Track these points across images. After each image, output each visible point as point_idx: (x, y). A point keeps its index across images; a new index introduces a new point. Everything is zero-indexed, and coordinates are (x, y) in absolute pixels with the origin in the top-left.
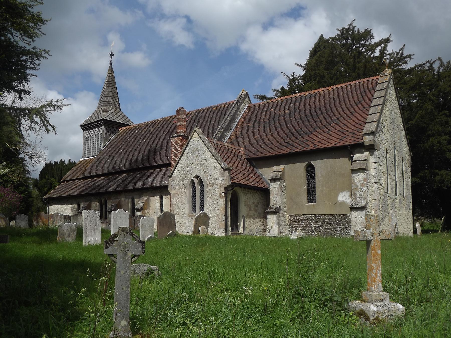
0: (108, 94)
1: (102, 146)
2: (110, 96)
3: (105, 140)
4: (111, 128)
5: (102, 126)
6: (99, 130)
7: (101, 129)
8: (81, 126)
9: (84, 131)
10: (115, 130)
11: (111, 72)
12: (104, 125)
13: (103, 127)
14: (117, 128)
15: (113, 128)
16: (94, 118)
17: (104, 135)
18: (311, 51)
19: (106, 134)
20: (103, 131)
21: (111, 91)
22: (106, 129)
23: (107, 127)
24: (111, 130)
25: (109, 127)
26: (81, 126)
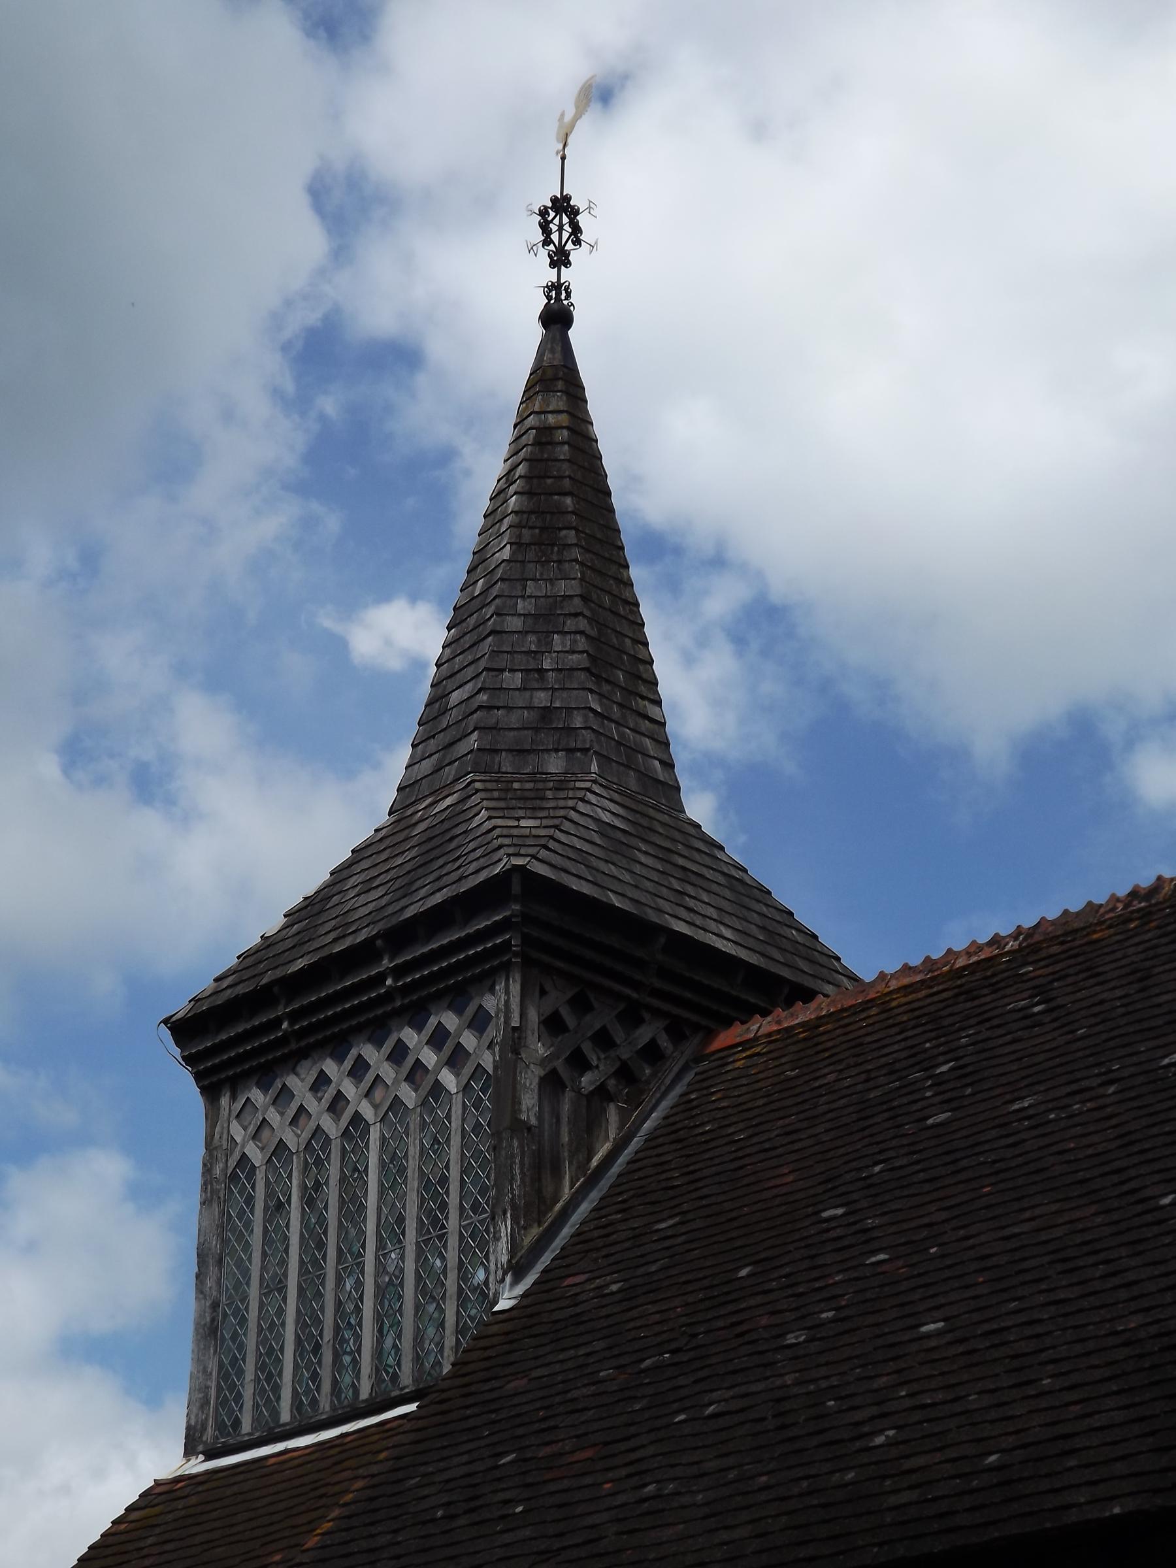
0: (546, 620)
1: (501, 1253)
2: (566, 649)
3: (544, 1165)
4: (603, 1017)
5: (486, 981)
6: (438, 1039)
7: (479, 1022)
8: (184, 1029)
9: (210, 1090)
10: (652, 1053)
11: (557, 402)
12: (528, 963)
13: (503, 999)
14: (677, 1031)
15: (632, 1017)
16: (363, 905)
17: (529, 1102)
18: (1066, 912)
19: (552, 1083)
20: (514, 1041)
21: (571, 587)
22: (553, 1025)
23: (557, 999)
24: (603, 1040)
25: (581, 1005)
26: (184, 1029)
